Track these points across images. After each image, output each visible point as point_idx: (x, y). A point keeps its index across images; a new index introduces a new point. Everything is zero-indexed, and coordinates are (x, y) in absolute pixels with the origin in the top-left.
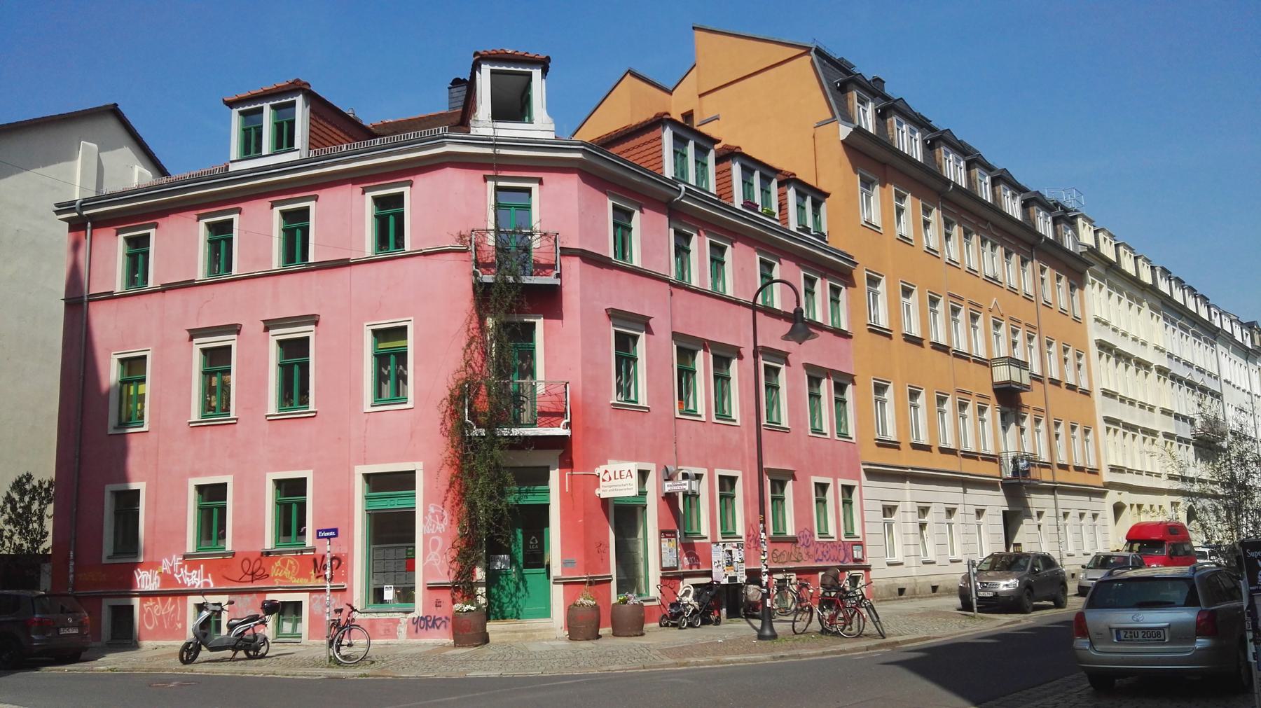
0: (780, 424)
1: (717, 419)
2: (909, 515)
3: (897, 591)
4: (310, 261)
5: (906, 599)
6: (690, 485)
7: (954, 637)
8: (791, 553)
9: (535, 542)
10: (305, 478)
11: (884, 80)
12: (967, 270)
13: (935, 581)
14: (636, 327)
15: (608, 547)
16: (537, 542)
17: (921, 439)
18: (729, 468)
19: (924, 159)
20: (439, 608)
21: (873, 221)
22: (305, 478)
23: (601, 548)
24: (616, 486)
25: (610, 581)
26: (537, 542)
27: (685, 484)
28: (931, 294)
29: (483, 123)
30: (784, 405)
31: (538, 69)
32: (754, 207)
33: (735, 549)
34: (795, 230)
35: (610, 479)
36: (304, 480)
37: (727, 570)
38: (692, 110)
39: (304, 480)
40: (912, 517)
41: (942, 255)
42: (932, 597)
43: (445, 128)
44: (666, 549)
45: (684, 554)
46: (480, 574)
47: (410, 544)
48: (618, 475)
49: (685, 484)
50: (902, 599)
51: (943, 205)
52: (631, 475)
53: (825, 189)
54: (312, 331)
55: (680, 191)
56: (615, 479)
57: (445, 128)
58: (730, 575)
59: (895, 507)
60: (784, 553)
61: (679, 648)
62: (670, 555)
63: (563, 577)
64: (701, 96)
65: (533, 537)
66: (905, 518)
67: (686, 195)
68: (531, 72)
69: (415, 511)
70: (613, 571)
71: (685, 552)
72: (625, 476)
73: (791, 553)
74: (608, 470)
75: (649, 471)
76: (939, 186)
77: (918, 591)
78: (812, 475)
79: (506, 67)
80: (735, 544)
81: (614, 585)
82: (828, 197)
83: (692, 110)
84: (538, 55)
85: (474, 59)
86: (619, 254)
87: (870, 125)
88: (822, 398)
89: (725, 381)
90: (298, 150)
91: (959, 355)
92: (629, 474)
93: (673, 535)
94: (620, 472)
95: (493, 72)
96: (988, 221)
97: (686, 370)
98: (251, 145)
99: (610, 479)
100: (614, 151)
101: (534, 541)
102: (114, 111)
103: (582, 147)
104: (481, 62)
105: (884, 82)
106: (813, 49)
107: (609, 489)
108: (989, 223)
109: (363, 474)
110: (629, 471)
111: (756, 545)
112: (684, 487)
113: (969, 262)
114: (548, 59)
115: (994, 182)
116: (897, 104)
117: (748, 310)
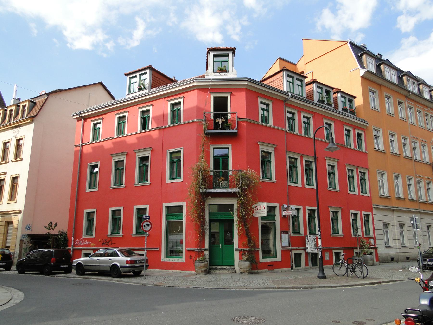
0: (271, 179)
2: (396, 227)
3: (390, 258)
4: (150, 128)
5: (395, 262)
6: (293, 213)
9: (229, 234)
11: (382, 55)
12: (419, 126)
13: (408, 255)
16: (230, 234)
17: (385, 194)
19: (398, 83)
20: (191, 259)
21: (376, 107)
26: (230, 234)
27: (291, 212)
28: (390, 132)
30: (273, 172)
32: (323, 102)
34: (341, 111)
35: (257, 209)
38: (304, 71)
40: (397, 228)
42: (407, 262)
47: (181, 234)
48: (260, 208)
50: (392, 262)
51: (408, 101)
52: (264, 208)
53: (354, 95)
54: (150, 154)
55: (289, 96)
56: (259, 209)
59: (389, 224)
61: (281, 280)
63: (239, 249)
64: (305, 64)
65: (228, 232)
66: (394, 228)
67: (291, 97)
69: (183, 221)
75: (276, 207)
76: (405, 93)
77: (400, 259)
83: (304, 71)
84: (231, 47)
85: (207, 51)
87: (373, 69)
88: (272, 163)
89: (311, 171)
90: (148, 89)
91: (417, 161)
92: (264, 207)
93: (287, 233)
94: (261, 206)
96: (428, 107)
97: (309, 169)
99: (257, 209)
100: (264, 82)
101: (228, 234)
102: (101, 84)
103: (247, 80)
104: (209, 51)
105: (382, 56)
106: (349, 42)
108: (429, 108)
109: (166, 206)
110: (264, 206)
113: (411, 120)
114: (235, 48)
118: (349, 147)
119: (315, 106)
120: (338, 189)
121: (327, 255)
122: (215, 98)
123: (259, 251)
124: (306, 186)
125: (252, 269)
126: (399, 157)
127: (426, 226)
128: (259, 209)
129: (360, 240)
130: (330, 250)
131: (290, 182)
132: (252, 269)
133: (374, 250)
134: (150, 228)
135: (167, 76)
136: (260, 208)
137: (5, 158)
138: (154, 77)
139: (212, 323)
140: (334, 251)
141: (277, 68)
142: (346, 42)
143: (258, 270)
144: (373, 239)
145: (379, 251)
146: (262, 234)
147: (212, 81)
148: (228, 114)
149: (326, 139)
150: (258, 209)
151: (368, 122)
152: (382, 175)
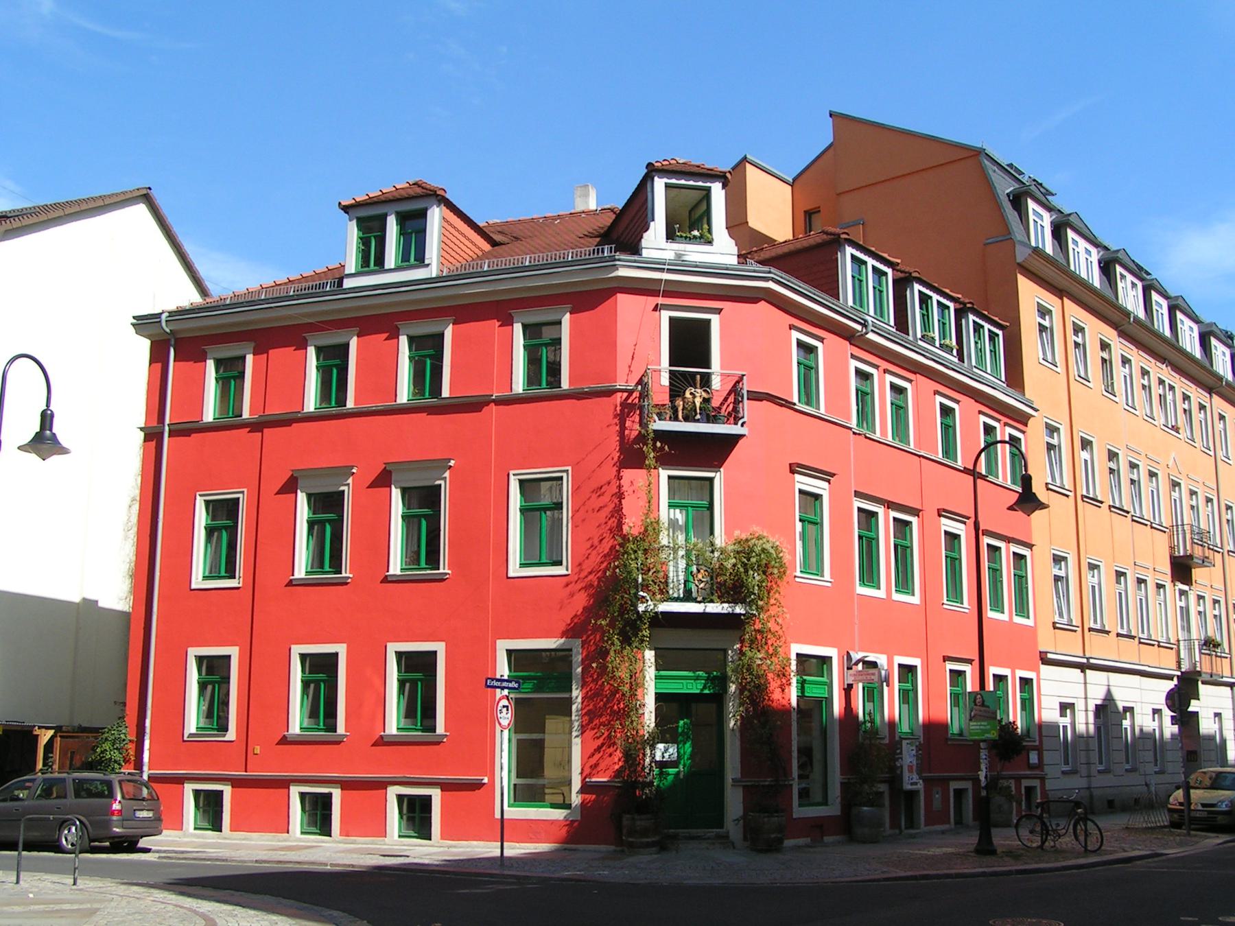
4: (443, 396)
10: (436, 652)
22: (436, 652)
27: (873, 674)
29: (655, 241)
31: (717, 183)
36: (336, 654)
39: (336, 654)
41: (1120, 400)
43: (611, 248)
46: (626, 778)
57: (611, 248)
68: (710, 187)
78: (348, 647)
79: (686, 180)
86: (803, 399)
95: (667, 186)
98: (372, 257)
104: (654, 174)
112: (873, 677)
115: (1172, 310)
116: (1071, 218)
117: (969, 476)
118: (991, 478)
119: (1010, 398)
120: (829, 580)
121: (937, 796)
122: (671, 319)
123: (791, 785)
124: (897, 597)
126: (1100, 507)
127: (1058, 707)
130: (945, 781)
131: (896, 590)
133: (971, 782)
134: (510, 718)
138: (446, 225)
140: (954, 785)
142: (975, 153)
143: (497, 853)
144: (1036, 752)
145: (1049, 785)
147: (668, 269)
148: (713, 377)
149: (940, 455)
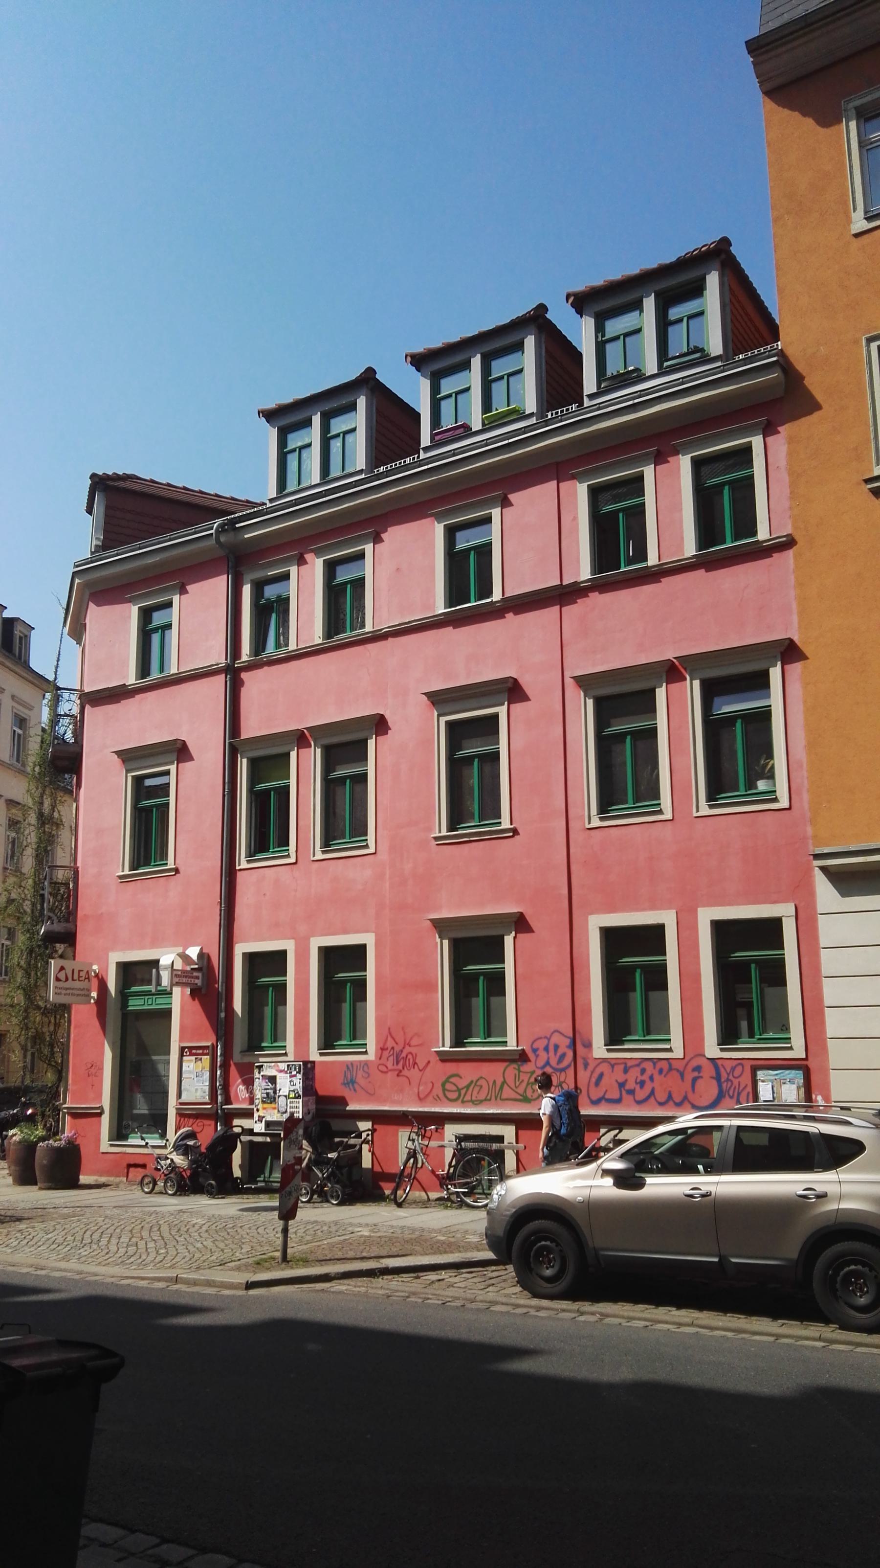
1: (601, 819)
7: (64, 1274)
8: (504, 1082)
14: (159, 762)
15: (101, 1069)
18: (345, 931)
23: (93, 1070)
24: (73, 989)
25: (100, 1115)
27: (197, 978)
33: (282, 1074)
35: (67, 979)
37: (264, 1109)
44: (189, 1072)
45: (240, 1080)
48: (76, 977)
49: (197, 978)
56: (73, 980)
58: (269, 1118)
60: (482, 1082)
62: (198, 1081)
70: (106, 1101)
71: (241, 1077)
72: (83, 978)
73: (504, 1082)
74: (65, 967)
80: (283, 1066)
81: (105, 1119)
82: (374, 372)
107: (64, 992)
111: (400, 1066)
112: (197, 981)
125: (262, 412)
128: (73, 980)
129: (858, 1279)
132: (262, 412)
135: (314, 394)
136: (76, 977)
137: (165, 668)
139: (77, 1232)
141: (273, 433)
146: (165, 1112)
150: (70, 979)
151: (108, 1145)
152: (142, 1238)
